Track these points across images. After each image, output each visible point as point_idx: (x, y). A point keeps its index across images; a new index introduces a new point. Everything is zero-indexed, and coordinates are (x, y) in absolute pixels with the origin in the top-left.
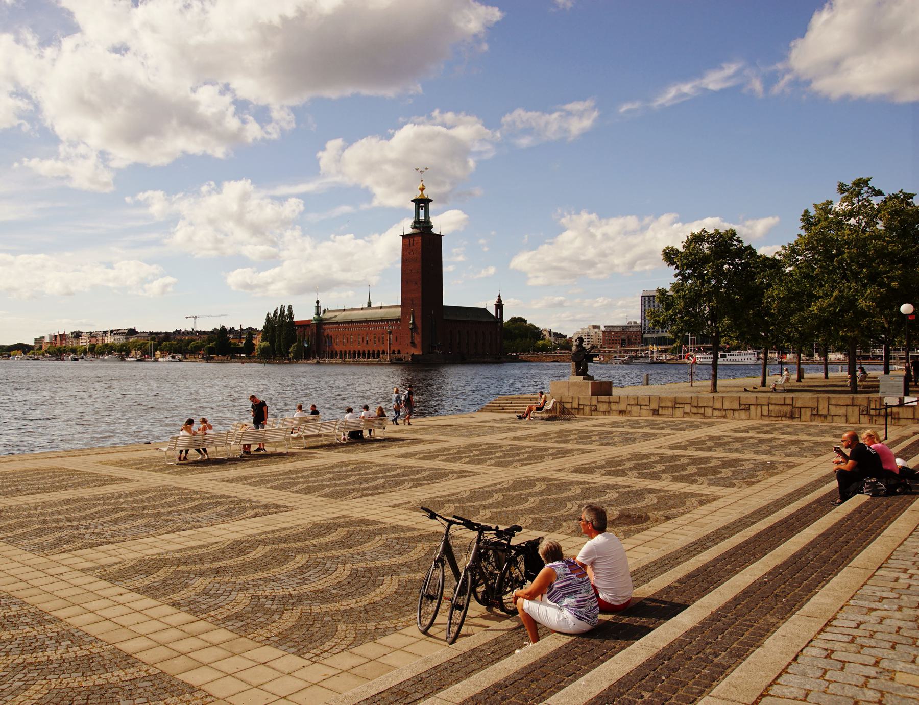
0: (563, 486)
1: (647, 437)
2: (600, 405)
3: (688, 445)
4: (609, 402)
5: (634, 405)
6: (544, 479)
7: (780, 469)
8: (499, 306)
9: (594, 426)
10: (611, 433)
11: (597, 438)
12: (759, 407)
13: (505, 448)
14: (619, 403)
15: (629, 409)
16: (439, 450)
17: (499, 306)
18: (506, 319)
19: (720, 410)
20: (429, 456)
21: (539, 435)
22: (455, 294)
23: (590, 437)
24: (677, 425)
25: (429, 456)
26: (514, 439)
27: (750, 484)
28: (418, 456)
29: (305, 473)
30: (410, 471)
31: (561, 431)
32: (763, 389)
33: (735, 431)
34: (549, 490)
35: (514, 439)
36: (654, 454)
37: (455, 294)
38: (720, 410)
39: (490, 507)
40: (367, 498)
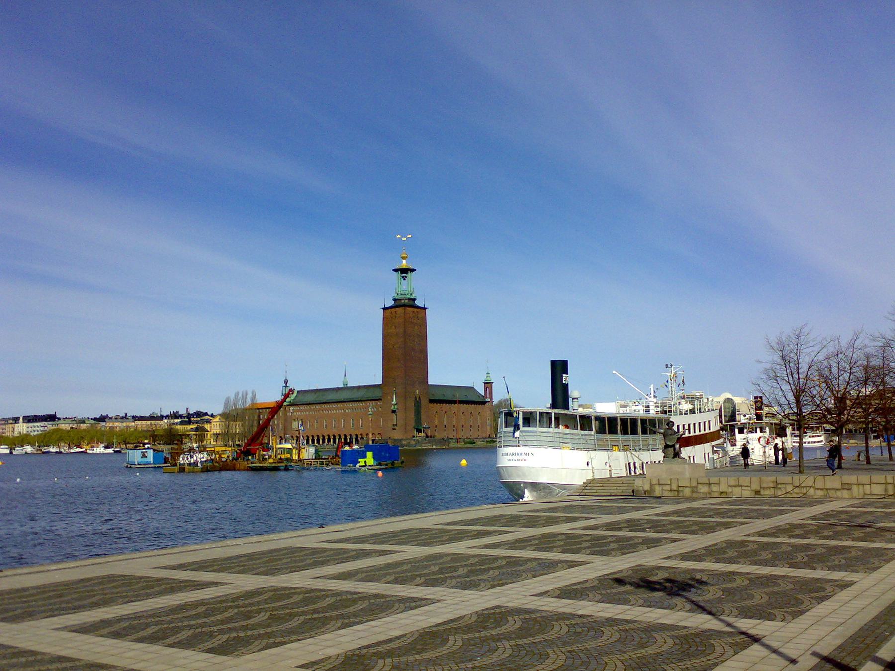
0: (546, 621)
1: (651, 543)
2: (700, 486)
3: (727, 548)
4: (709, 484)
5: (735, 486)
6: (518, 611)
7: (829, 590)
8: (488, 385)
9: (585, 528)
10: (605, 537)
11: (588, 544)
12: (861, 487)
13: (472, 561)
14: (719, 484)
15: (730, 490)
16: (388, 566)
17: (488, 385)
18: (496, 400)
19: (822, 489)
20: (371, 575)
21: (518, 541)
22: (440, 373)
23: (580, 543)
24: (687, 526)
25: (371, 575)
26: (486, 546)
27: (796, 614)
28: (360, 576)
29: (405, 567)
30: (345, 600)
31: (543, 536)
32: (868, 466)
33: (760, 535)
34: (523, 632)
35: (486, 546)
36: (660, 568)
37: (440, 373)
38: (822, 489)
39: (507, 637)
40: (354, 628)
